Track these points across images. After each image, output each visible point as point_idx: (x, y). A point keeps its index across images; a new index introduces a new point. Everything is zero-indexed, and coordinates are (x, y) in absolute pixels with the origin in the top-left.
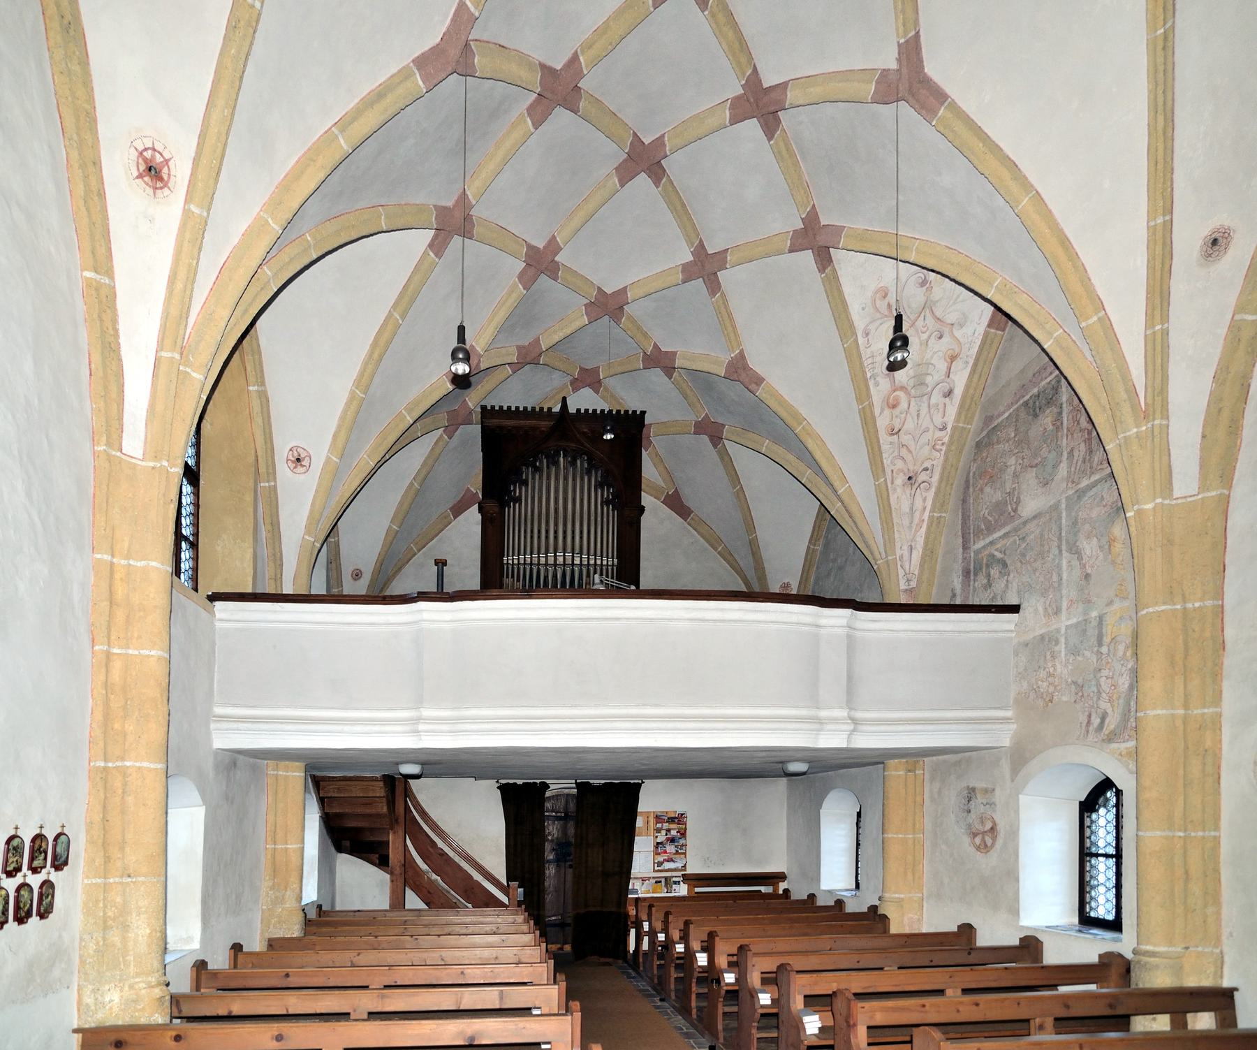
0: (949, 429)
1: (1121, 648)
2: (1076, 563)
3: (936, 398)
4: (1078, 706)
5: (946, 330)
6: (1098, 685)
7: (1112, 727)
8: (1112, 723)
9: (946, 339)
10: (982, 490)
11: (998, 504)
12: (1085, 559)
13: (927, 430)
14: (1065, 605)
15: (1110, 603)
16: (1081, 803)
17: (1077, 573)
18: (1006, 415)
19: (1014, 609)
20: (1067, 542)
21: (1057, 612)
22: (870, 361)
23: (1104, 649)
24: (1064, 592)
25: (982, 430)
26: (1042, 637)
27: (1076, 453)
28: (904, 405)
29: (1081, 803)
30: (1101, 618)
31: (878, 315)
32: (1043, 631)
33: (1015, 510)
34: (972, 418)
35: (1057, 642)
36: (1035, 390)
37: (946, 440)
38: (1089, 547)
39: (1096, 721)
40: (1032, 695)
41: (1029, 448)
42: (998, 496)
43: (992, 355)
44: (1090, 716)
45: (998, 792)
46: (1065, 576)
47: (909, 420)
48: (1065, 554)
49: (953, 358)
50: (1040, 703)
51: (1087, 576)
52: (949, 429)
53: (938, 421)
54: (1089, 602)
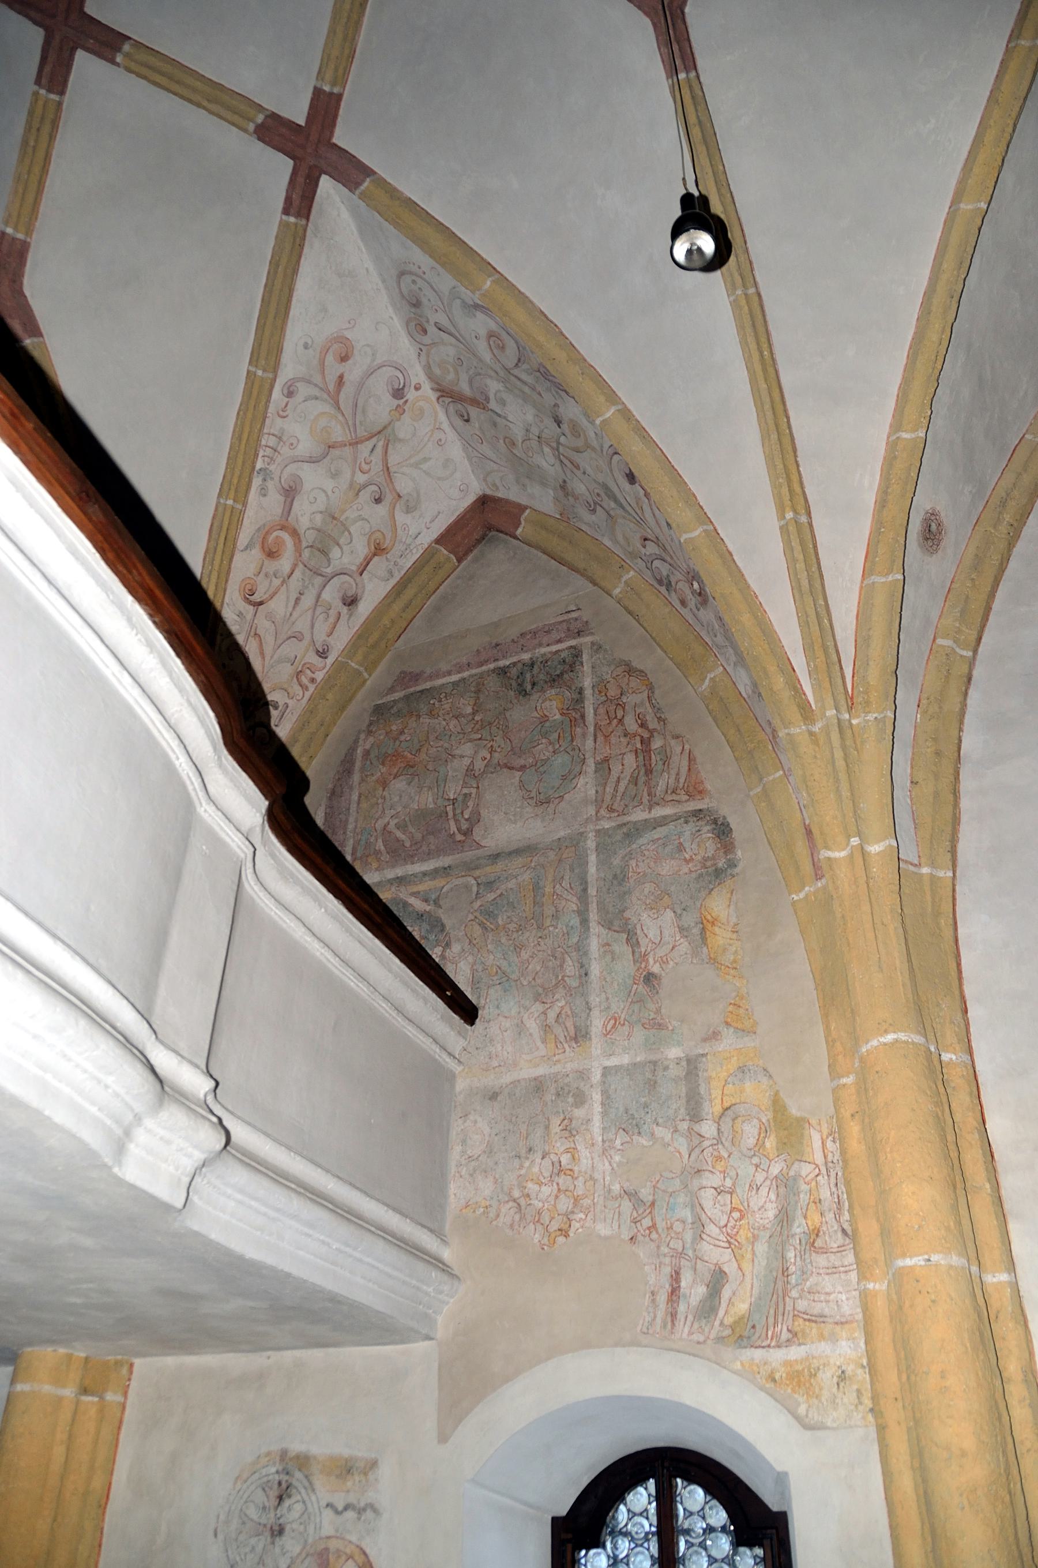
0: (330, 660)
1: (750, 1132)
2: (621, 947)
3: (331, 595)
4: (642, 1252)
5: (389, 498)
6: (695, 1205)
7: (742, 1307)
8: (739, 1300)
9: (382, 510)
10: (384, 784)
11: (422, 815)
12: (644, 945)
13: (298, 637)
14: (597, 1024)
15: (714, 1036)
16: (555, 1520)
17: (625, 967)
18: (455, 678)
19: (466, 1011)
20: (602, 908)
21: (580, 1036)
22: (272, 441)
23: (708, 1128)
24: (594, 999)
25: (392, 690)
26: (538, 1086)
27: (616, 769)
28: (285, 564)
29: (555, 1520)
30: (692, 1066)
31: (317, 379)
32: (541, 1071)
33: (467, 833)
34: (375, 664)
35: (580, 1099)
36: (526, 657)
37: (319, 676)
38: (656, 927)
39: (694, 1292)
40: (508, 1211)
41: (506, 737)
42: (427, 800)
43: (432, 585)
44: (676, 1277)
45: (386, 1472)
46: (595, 969)
47: (282, 596)
48: (595, 928)
49: (379, 550)
50: (534, 1235)
51: (650, 978)
52: (330, 660)
53: (320, 637)
54: (660, 1026)
